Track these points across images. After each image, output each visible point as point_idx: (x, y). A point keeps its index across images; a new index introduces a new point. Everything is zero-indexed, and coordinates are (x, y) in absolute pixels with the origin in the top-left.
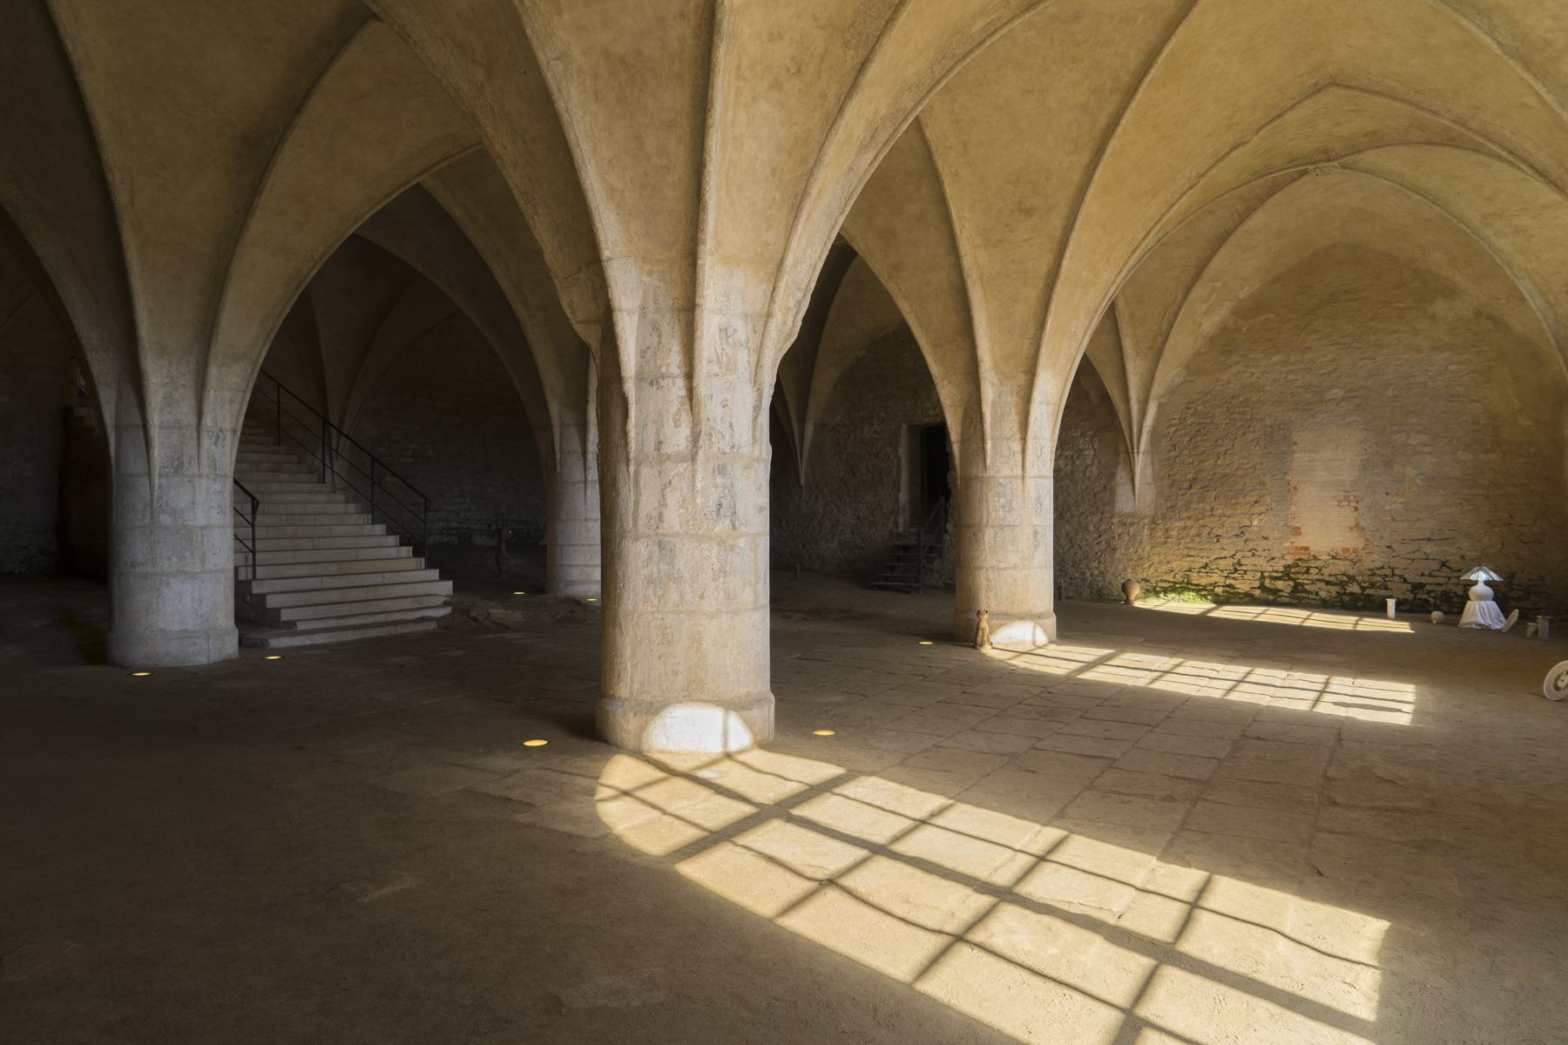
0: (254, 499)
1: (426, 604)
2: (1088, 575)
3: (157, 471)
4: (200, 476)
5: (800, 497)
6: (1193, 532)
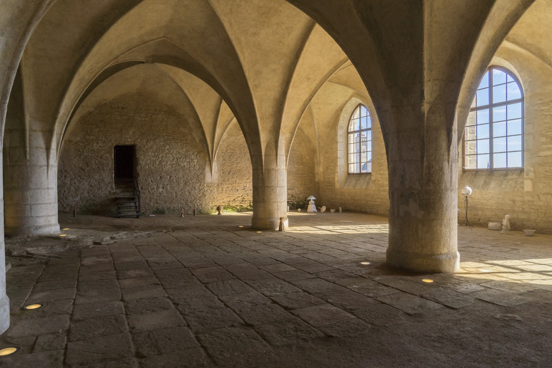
2: (196, 205)
6: (230, 188)
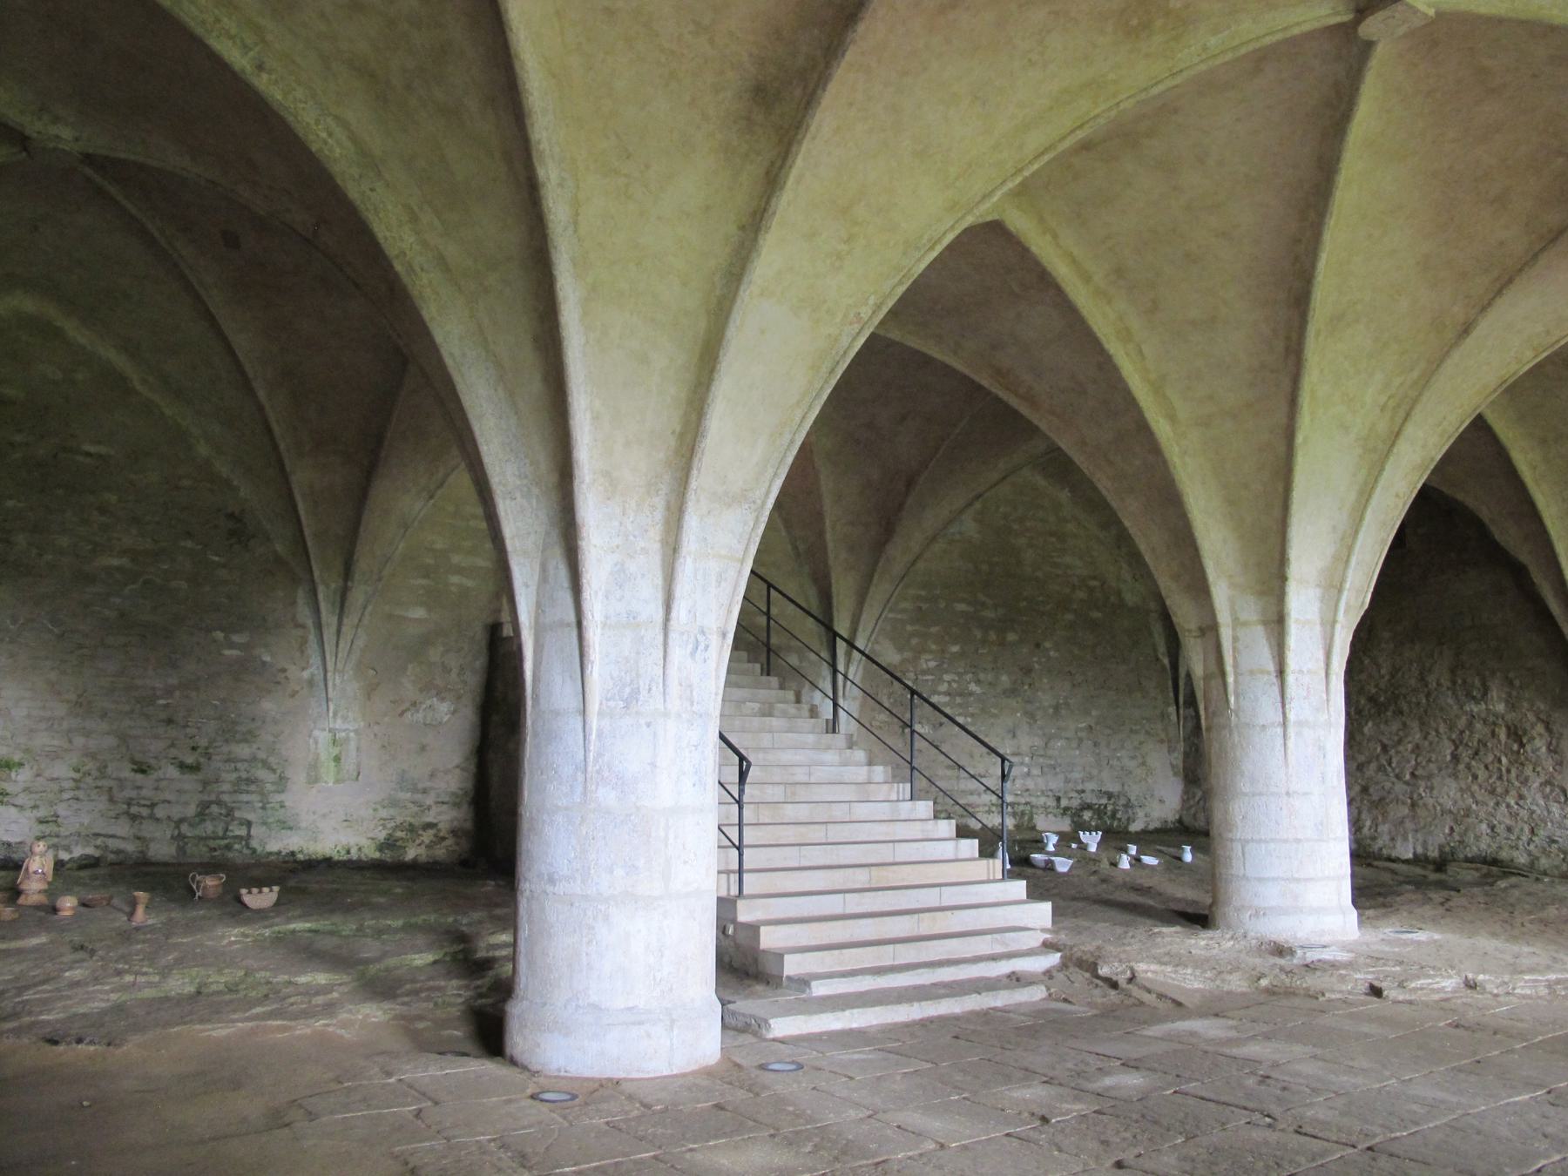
0: (742, 758)
1: (1014, 947)
3: (596, 707)
4: (666, 715)
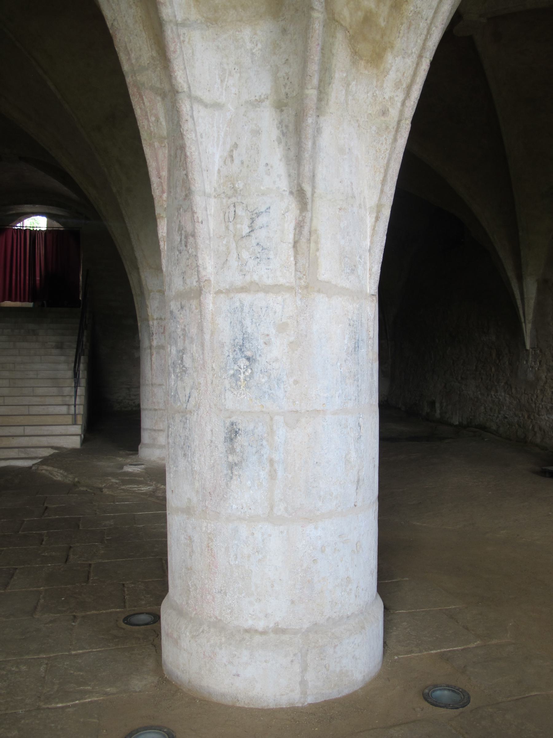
5: (527, 361)
